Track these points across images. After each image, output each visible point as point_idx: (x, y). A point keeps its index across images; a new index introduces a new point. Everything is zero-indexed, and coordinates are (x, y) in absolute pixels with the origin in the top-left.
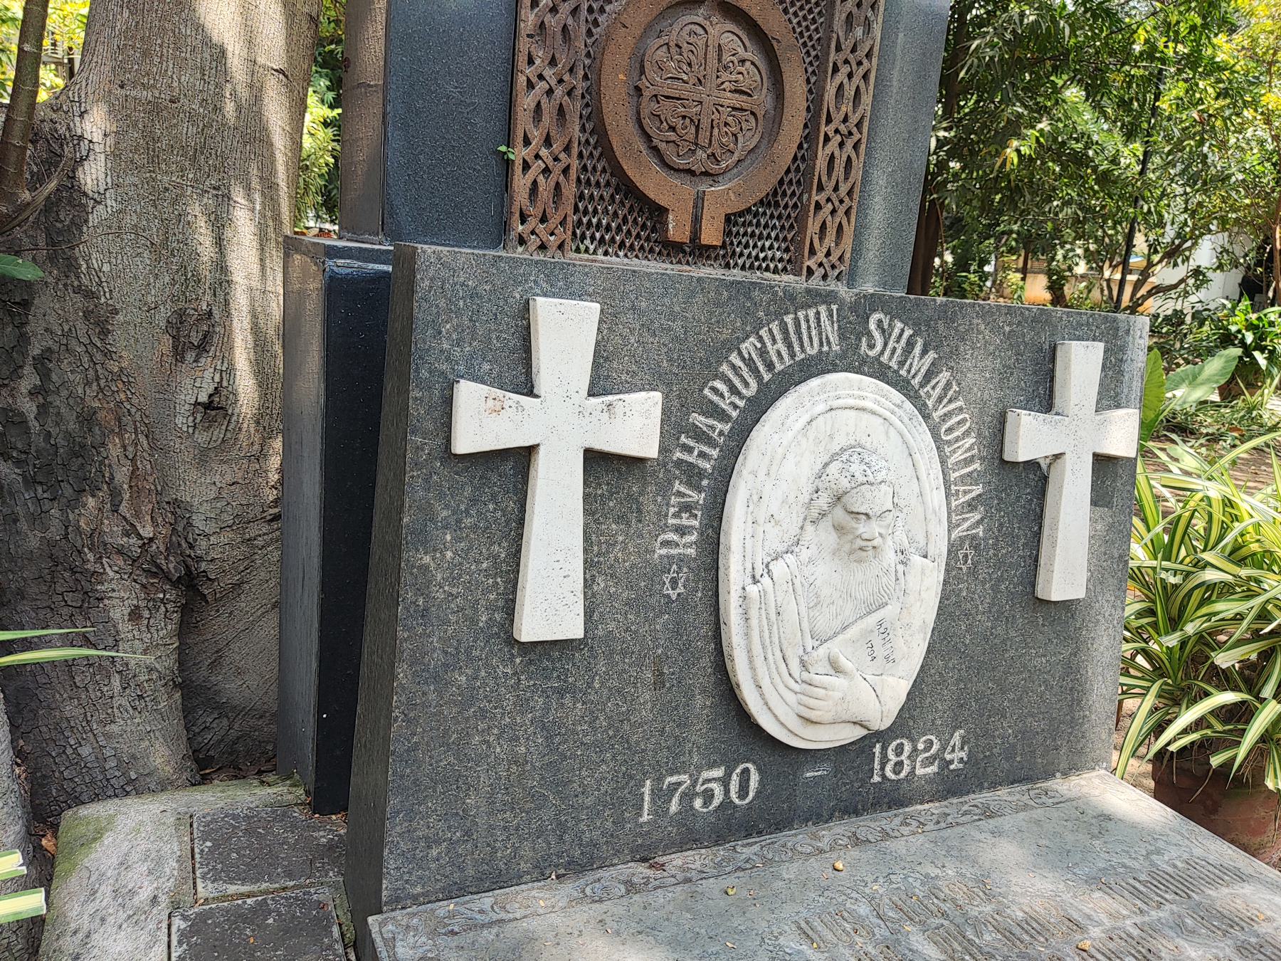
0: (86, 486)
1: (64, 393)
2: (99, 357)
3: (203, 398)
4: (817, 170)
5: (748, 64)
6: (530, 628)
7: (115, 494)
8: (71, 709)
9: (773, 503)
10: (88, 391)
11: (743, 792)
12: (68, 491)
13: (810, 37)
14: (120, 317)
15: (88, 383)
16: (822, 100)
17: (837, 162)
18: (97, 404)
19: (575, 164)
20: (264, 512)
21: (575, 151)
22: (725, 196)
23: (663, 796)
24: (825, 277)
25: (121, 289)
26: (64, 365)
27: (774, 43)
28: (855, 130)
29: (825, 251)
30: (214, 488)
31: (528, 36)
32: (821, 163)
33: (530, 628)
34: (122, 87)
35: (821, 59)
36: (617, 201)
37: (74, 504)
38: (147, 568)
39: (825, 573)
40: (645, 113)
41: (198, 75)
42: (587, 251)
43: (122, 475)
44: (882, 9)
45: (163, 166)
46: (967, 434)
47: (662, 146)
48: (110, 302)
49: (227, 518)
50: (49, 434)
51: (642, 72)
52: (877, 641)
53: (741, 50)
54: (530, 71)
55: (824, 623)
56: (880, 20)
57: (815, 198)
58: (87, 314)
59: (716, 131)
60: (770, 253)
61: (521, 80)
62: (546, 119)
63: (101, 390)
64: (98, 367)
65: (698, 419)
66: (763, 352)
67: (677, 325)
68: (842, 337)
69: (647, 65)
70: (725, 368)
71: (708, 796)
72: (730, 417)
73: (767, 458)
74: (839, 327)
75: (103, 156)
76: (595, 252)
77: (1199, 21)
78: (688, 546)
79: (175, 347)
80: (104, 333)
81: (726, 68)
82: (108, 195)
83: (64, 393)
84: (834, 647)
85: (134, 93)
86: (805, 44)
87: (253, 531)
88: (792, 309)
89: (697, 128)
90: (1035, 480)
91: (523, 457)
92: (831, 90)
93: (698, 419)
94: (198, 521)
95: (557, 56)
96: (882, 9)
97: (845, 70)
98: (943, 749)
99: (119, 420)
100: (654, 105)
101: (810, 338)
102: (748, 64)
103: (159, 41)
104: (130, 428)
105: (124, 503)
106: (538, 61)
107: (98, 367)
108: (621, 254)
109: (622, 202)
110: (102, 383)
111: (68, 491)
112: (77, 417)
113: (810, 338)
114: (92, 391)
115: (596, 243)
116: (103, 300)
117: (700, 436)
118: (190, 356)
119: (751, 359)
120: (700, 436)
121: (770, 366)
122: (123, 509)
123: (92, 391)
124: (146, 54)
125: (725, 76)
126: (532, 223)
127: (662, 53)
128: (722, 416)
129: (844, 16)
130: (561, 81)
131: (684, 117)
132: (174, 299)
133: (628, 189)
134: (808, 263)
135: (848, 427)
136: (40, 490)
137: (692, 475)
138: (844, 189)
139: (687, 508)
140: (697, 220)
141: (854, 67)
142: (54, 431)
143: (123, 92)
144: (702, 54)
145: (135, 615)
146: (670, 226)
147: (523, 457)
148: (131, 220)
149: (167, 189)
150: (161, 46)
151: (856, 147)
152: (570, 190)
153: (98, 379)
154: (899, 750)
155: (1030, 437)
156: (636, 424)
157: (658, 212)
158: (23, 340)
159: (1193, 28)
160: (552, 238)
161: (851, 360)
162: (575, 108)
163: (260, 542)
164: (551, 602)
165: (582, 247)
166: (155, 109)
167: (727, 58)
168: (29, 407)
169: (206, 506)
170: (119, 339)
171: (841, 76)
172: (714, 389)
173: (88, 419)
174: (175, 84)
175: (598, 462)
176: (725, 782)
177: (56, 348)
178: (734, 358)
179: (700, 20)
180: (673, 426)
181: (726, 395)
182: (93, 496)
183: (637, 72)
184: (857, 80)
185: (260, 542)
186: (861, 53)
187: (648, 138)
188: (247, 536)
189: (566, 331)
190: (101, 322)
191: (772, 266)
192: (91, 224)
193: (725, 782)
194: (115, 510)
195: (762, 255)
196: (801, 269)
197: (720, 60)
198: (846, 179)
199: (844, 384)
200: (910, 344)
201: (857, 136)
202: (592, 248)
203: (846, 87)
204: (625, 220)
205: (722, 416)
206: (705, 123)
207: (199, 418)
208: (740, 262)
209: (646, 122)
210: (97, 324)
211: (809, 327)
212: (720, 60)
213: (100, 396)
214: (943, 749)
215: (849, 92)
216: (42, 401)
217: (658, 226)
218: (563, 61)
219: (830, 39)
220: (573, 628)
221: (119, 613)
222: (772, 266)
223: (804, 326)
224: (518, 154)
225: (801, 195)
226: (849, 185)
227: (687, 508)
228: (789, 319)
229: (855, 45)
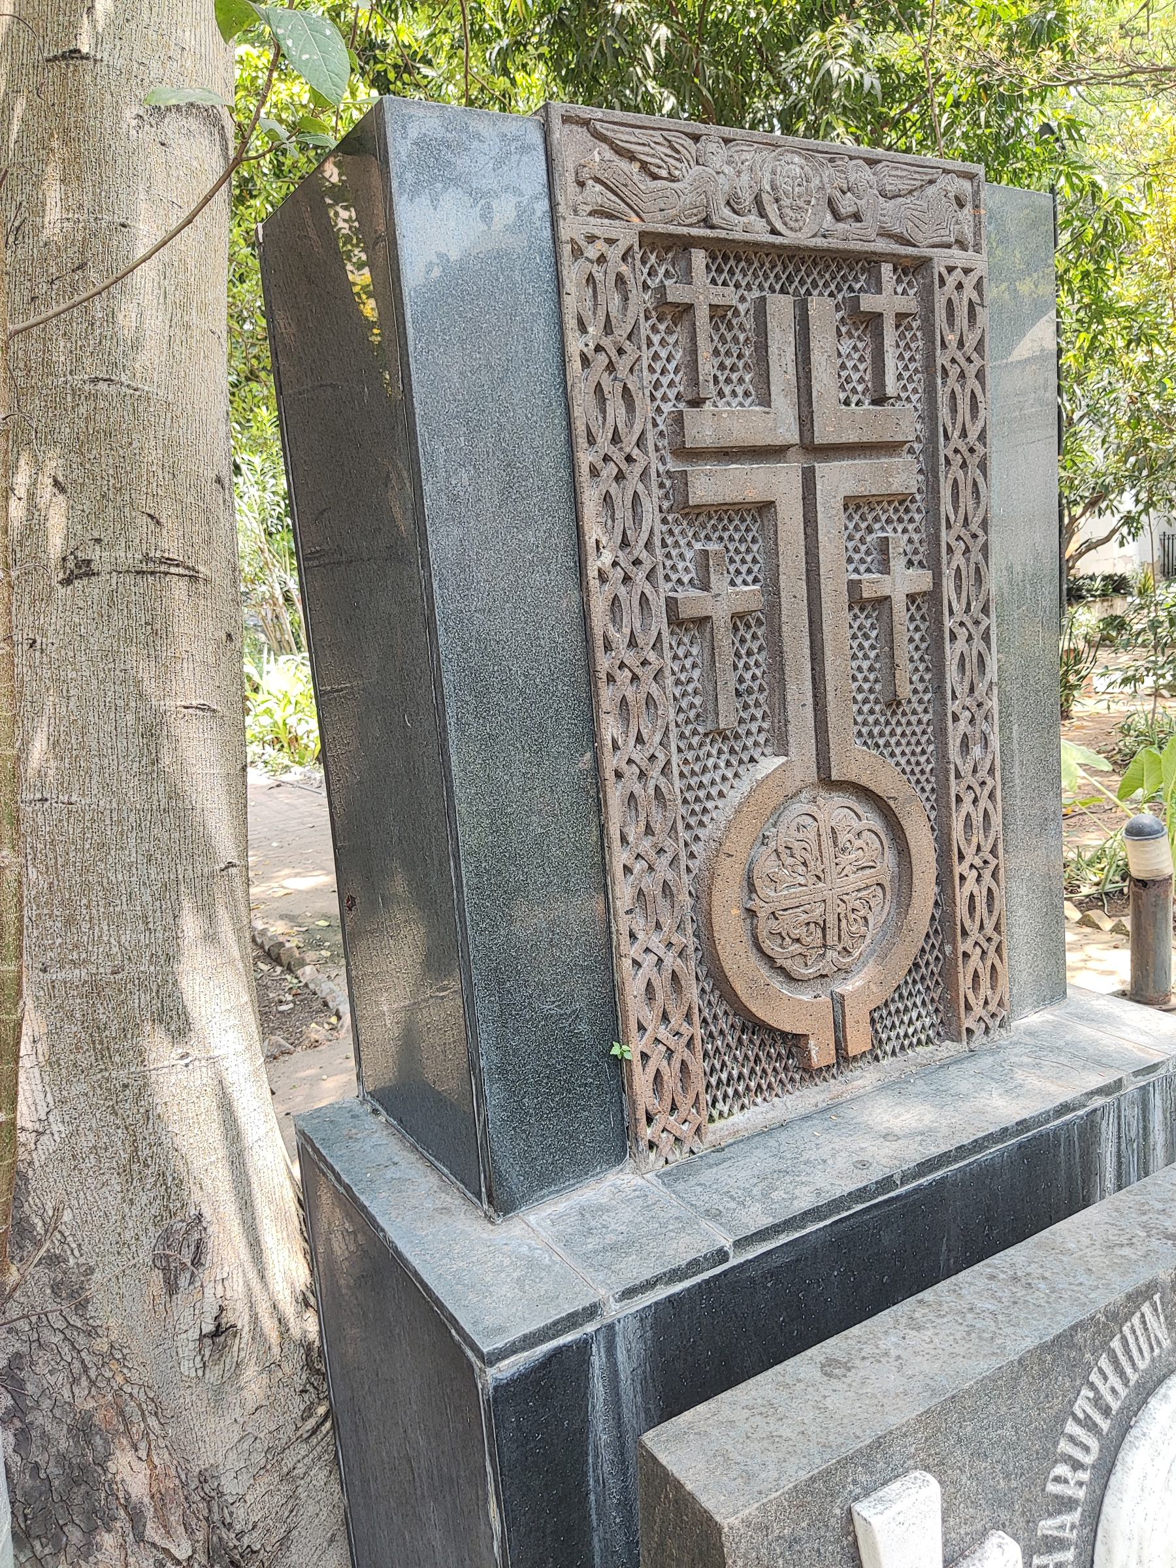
1: (46, 1404)
2: (81, 1340)
3: (209, 1328)
4: (958, 915)
5: (866, 834)
10: (76, 1390)
12: (75, 1536)
13: (922, 772)
14: (97, 1276)
15: (75, 1381)
16: (950, 840)
17: (978, 900)
18: (91, 1404)
19: (699, 1032)
20: (297, 1429)
21: (696, 1019)
22: (861, 986)
24: (987, 1030)
25: (91, 1237)
26: (41, 1368)
27: (891, 802)
28: (990, 858)
29: (982, 1003)
30: (236, 1427)
31: (627, 913)
32: (962, 908)
34: (44, 971)
35: (941, 790)
36: (746, 1042)
40: (763, 935)
41: (142, 927)
42: (721, 1114)
44: (996, 716)
45: (117, 1059)
47: (787, 964)
48: (82, 1260)
49: (259, 1458)
50: (37, 1466)
51: (752, 888)
53: (855, 823)
54: (635, 951)
56: (996, 729)
57: (962, 948)
58: (56, 1288)
59: (844, 922)
60: (918, 1024)
62: (660, 996)
63: (93, 1383)
64: (83, 1354)
67: (1008, 1433)
69: (757, 883)
70: (1064, 1446)
72: (1076, 1501)
73: (1135, 1543)
74: (1166, 1318)
75: (36, 1070)
76: (730, 1113)
77: (1091, 267)
79: (167, 1281)
80: (81, 1306)
81: (843, 850)
82: (51, 1118)
83: (46, 1404)
85: (61, 975)
86: (918, 782)
87: (289, 1460)
88: (1117, 1329)
89: (824, 929)
92: (958, 826)
94: (231, 1487)
95: (661, 920)
96: (996, 716)
97: (968, 798)
99: (122, 1413)
100: (773, 923)
101: (1140, 1350)
102: (866, 834)
103: (84, 901)
104: (137, 1418)
105: (149, 1525)
106: (641, 936)
107: (83, 1354)
108: (759, 1100)
109: (751, 1041)
110: (93, 1373)
111: (75, 1536)
112: (69, 1431)
113: (1140, 1350)
114: (81, 1390)
115: (729, 1102)
116: (72, 1262)
118: (183, 1281)
119: (1088, 1416)
122: (152, 1532)
123: (81, 1390)
124: (69, 922)
125: (844, 859)
126: (660, 1120)
127: (773, 861)
129: (959, 741)
130: (670, 945)
131: (808, 924)
132: (157, 1221)
133: (753, 1026)
134: (966, 1025)
136: (38, 1547)
140: (839, 1028)
141: (978, 790)
142: (41, 1459)
143: (47, 976)
144: (815, 847)
146: (813, 1053)
148: (85, 1143)
149: (126, 1086)
150: (87, 907)
151: (994, 875)
152: (698, 1066)
153: (86, 1369)
157: (795, 1043)
159: (1086, 274)
160: (685, 1127)
162: (688, 970)
163: (299, 1471)
165: (715, 1113)
166: (94, 989)
167: (843, 839)
169: (232, 1456)
170: (101, 1310)
171: (967, 806)
172: (1057, 1479)
173: (83, 1429)
174: (115, 950)
177: (25, 1349)
178: (1071, 1428)
179: (807, 808)
181: (1069, 1475)
182: (109, 1531)
183: (746, 890)
184: (984, 802)
185: (299, 1471)
186: (982, 773)
187: (770, 960)
188: (285, 1470)
190: (72, 1293)
191: (923, 1037)
192: (37, 1164)
194: (140, 1538)
195: (911, 1031)
196: (960, 1033)
197: (836, 845)
198: (990, 911)
201: (993, 862)
202: (726, 1109)
203: (974, 816)
204: (757, 1060)
206: (832, 921)
207: (207, 1354)
208: (888, 1049)
209: (767, 945)
210: (71, 1296)
211: (1137, 1339)
212: (836, 845)
213: (93, 1392)
215: (978, 819)
216: (18, 1424)
217: (794, 1050)
218: (667, 923)
219: (947, 771)
222: (923, 1037)
223: (1131, 1340)
224: (630, 1050)
225: (942, 944)
226: (994, 918)
228: (1116, 1344)
229: (975, 766)
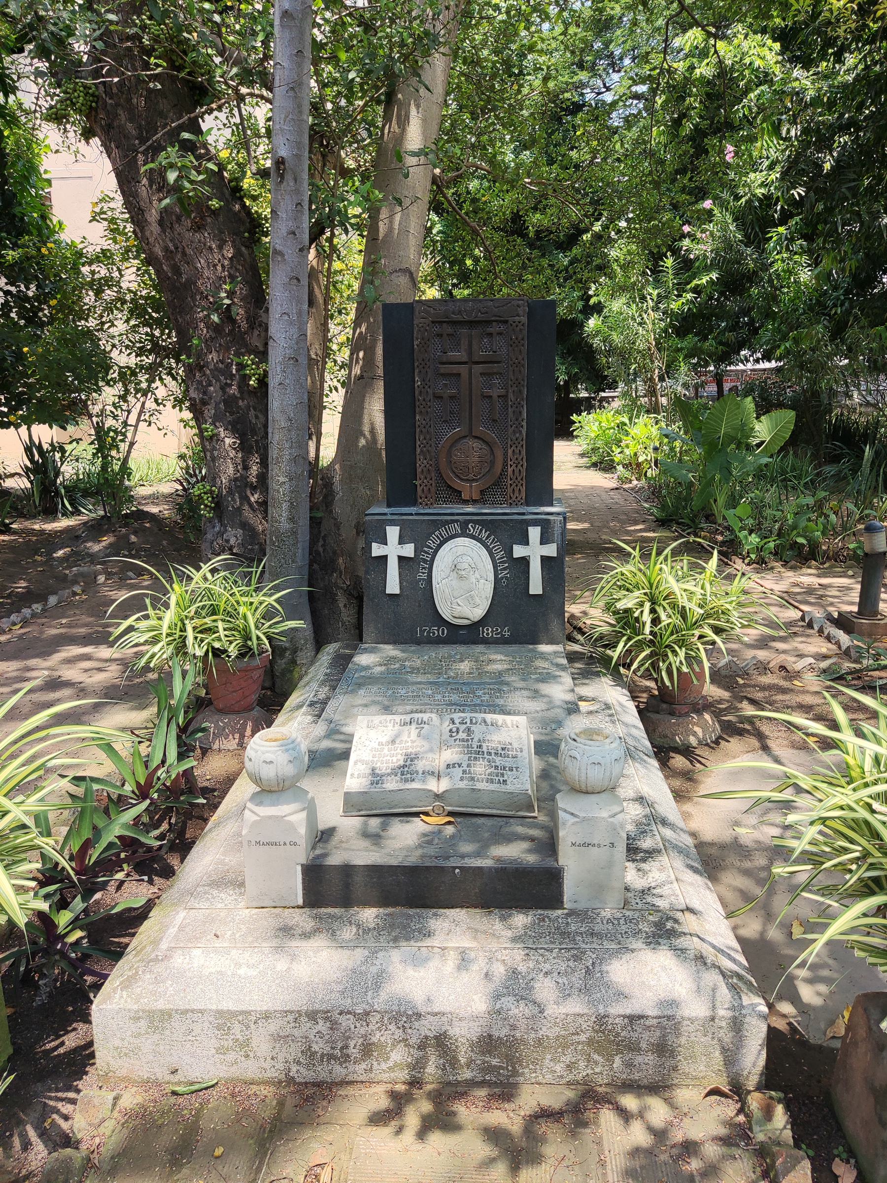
0: (334, 570)
6: (389, 591)
7: (341, 572)
8: (329, 630)
23: (422, 631)
33: (389, 591)
37: (331, 575)
38: (348, 593)
39: (455, 583)
43: (342, 568)
55: (456, 594)
78: (425, 576)
90: (525, 562)
91: (385, 557)
135: (461, 550)
137: (425, 561)
145: (345, 606)
147: (385, 557)
152: (433, 489)
155: (519, 551)
156: (409, 550)
158: (320, 532)
161: (464, 534)
164: (393, 586)
166: (351, 467)
168: (321, 550)
173: (335, 553)
175: (401, 558)
189: (393, 533)
190: (337, 526)
220: (397, 591)
221: (341, 605)
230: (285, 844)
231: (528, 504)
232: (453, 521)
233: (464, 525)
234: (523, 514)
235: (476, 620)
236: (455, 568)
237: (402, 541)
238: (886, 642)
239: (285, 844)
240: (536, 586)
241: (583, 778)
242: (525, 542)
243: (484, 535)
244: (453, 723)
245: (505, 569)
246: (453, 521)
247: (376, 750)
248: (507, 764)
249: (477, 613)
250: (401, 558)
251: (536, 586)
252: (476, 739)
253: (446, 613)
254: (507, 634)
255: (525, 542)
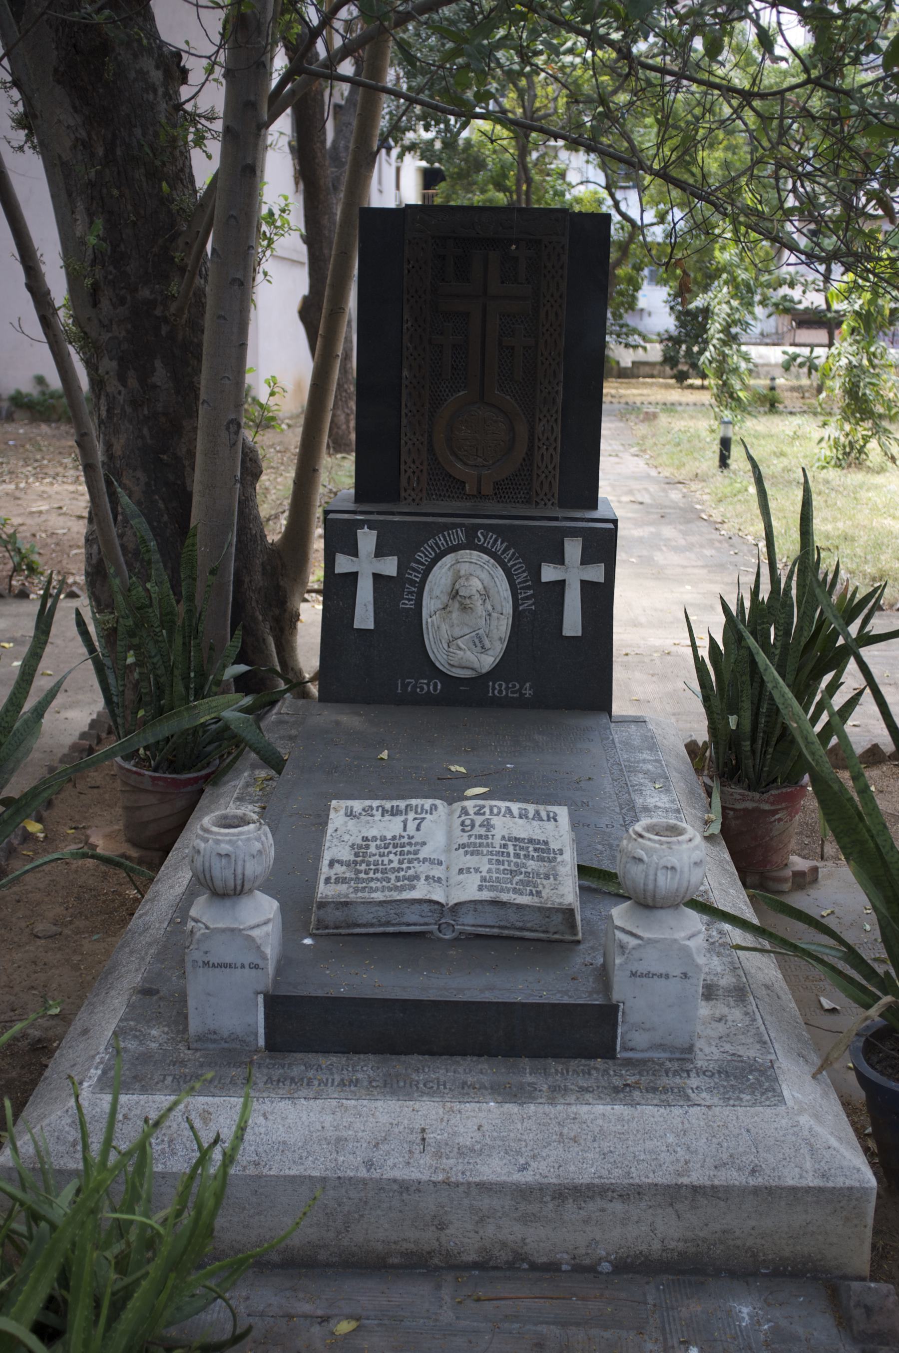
9: (437, 592)
11: (435, 689)
23: (405, 686)
46: (523, 572)
52: (477, 641)
61: (403, 442)
65: (414, 565)
66: (437, 544)
68: (467, 538)
71: (422, 689)
84: (459, 642)
91: (354, 576)
93: (414, 565)
98: (521, 688)
117: (414, 570)
120: (414, 570)
121: (439, 548)
126: (408, 492)
128: (423, 564)
137: (412, 583)
138: (550, 467)
139: (411, 593)
154: (500, 686)
156: (389, 566)
161: (471, 545)
175: (377, 577)
176: (428, 685)
180: (402, 567)
193: (428, 685)
199: (465, 554)
200: (496, 541)
205: (423, 564)
214: (521, 688)
227: (411, 593)
230: (243, 966)
231: (562, 505)
232: (455, 526)
233: (471, 532)
234: (556, 519)
235: (484, 671)
236: (454, 594)
237: (380, 553)
238: (898, 431)
239: (243, 966)
240: (573, 623)
241: (651, 886)
242: (559, 559)
243: (500, 546)
244: (467, 814)
245: (527, 598)
246: (455, 526)
247: (360, 847)
248: (542, 870)
249: (487, 662)
250: (377, 577)
251: (573, 623)
252: (498, 837)
253: (438, 654)
254: (528, 693)
255: (559, 559)
